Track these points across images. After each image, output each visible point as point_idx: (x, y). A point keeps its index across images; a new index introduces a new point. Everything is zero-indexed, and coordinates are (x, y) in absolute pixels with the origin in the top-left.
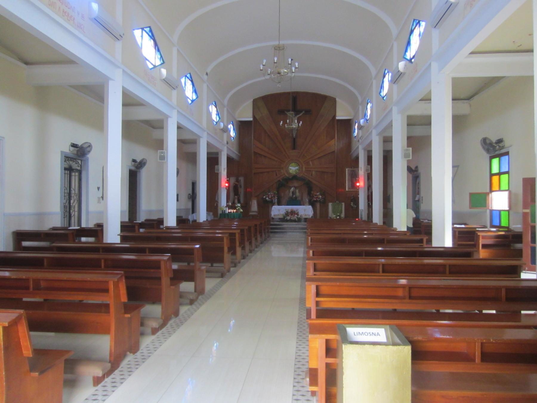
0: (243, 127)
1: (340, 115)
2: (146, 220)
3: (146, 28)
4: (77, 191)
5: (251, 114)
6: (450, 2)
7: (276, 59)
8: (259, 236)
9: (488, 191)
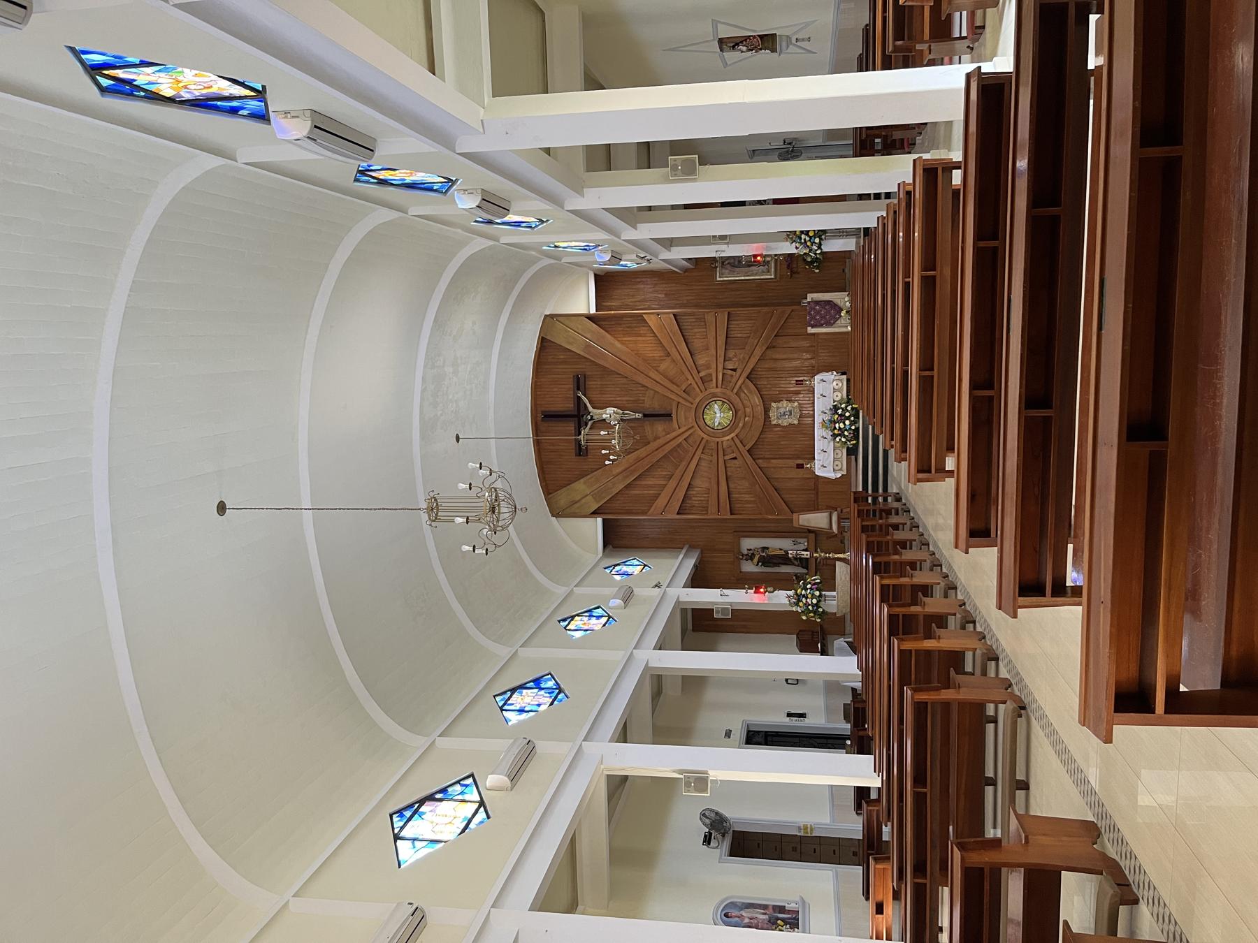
1: (583, 301)
2: (846, 718)
5: (589, 522)
6: (311, 131)
7: (459, 520)
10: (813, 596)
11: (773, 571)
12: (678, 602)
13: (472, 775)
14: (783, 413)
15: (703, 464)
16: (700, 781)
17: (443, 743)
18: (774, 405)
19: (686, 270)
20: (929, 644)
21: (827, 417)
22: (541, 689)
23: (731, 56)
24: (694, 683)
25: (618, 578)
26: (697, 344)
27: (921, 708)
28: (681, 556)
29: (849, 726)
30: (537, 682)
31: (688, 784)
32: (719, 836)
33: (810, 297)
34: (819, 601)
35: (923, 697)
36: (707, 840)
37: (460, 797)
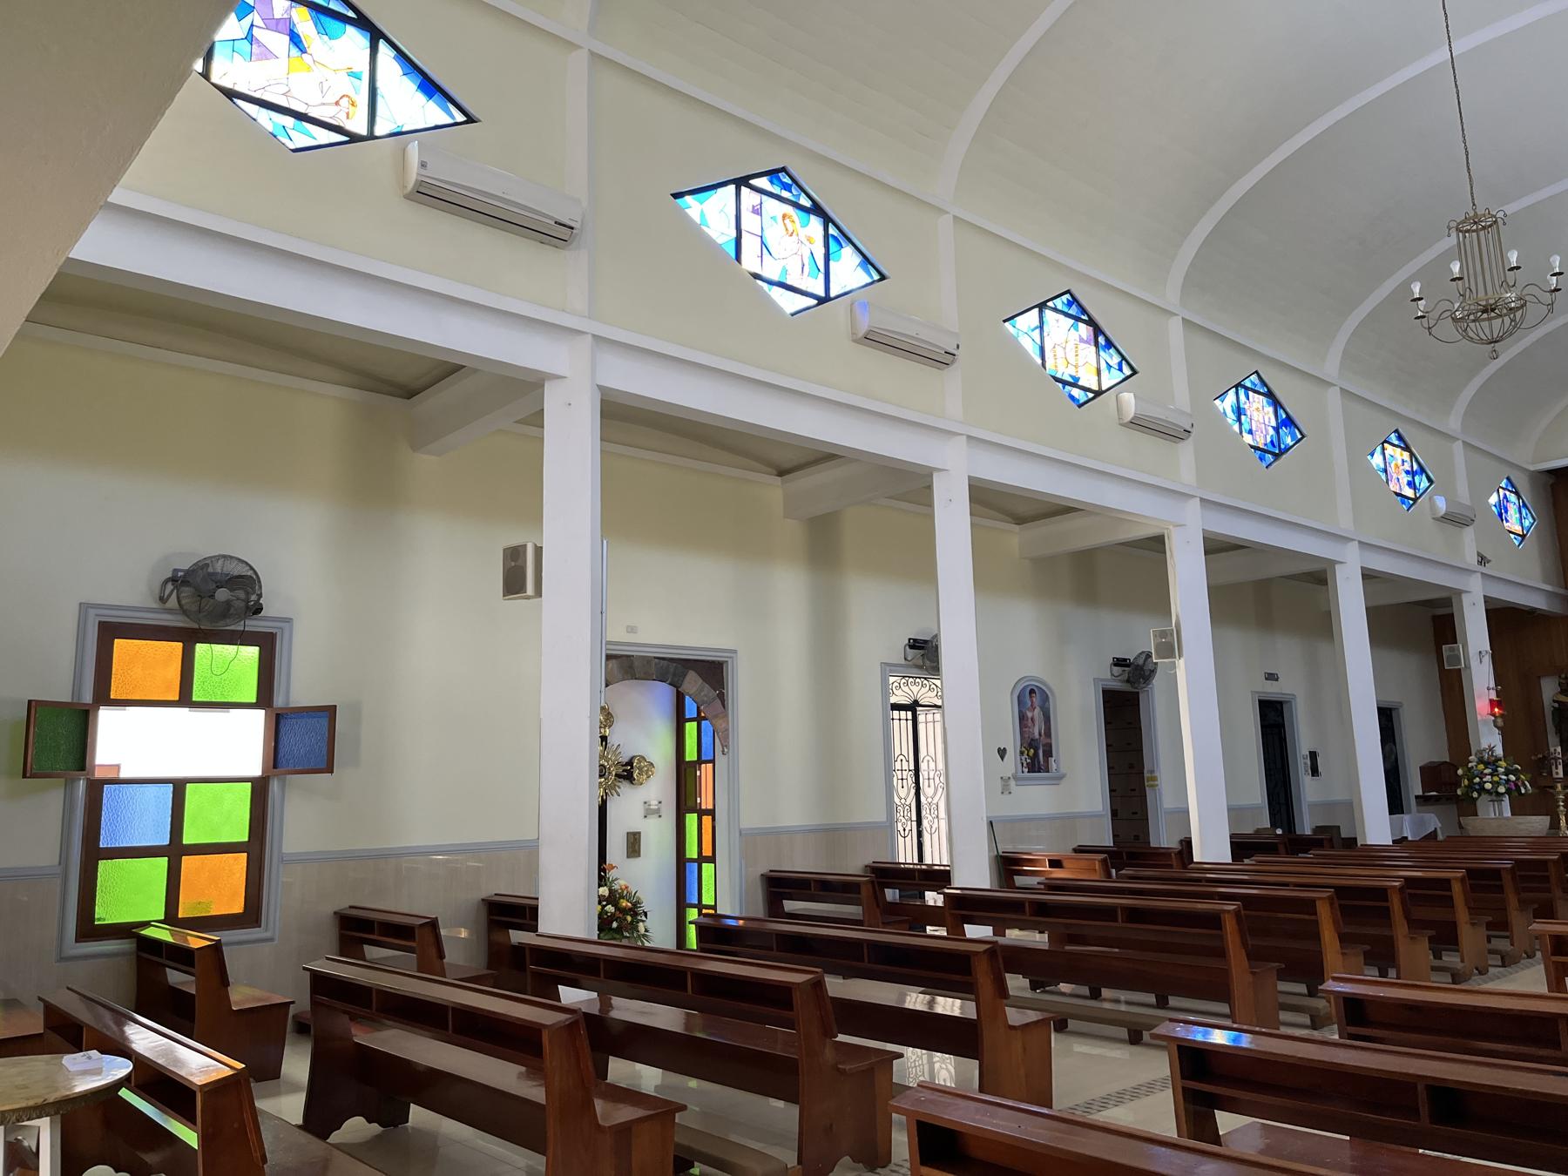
10: (1496, 784)
12: (1459, 593)
13: (1134, 372)
16: (1170, 648)
17: (1175, 327)
20: (1329, 936)
22: (1277, 429)
24: (1324, 625)
25: (1493, 499)
27: (1214, 921)
28: (1548, 588)
29: (1308, 832)
30: (1289, 422)
31: (1163, 634)
32: (1126, 676)
34: (1488, 792)
35: (1230, 925)
36: (1119, 662)
37: (1103, 366)
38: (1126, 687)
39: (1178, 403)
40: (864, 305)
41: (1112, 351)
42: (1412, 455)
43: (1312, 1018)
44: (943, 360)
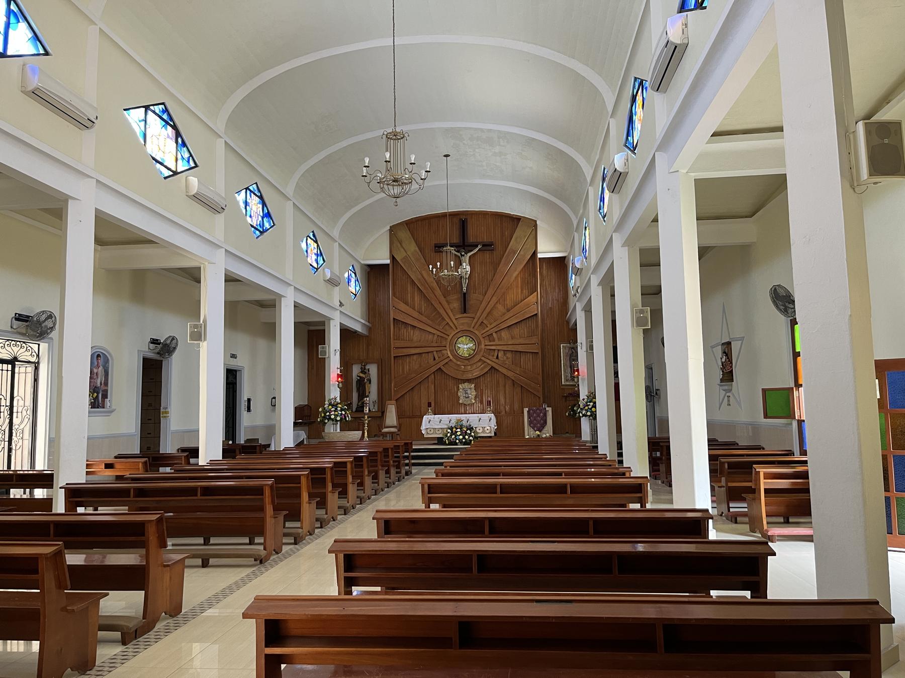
0: (374, 274)
1: (547, 249)
2: (248, 441)
3: (153, 105)
4: (29, 402)
5: (387, 254)
7: (388, 155)
8: (368, 481)
9: (792, 384)
10: (336, 416)
11: (353, 387)
13: (196, 166)
14: (467, 392)
15: (431, 336)
16: (198, 336)
18: (473, 386)
19: (568, 322)
20: (305, 496)
21: (464, 423)
22: (263, 218)
23: (719, 351)
24: (271, 331)
25: (346, 275)
26: (516, 331)
27: (259, 491)
28: (363, 321)
29: (242, 442)
30: (268, 215)
31: (196, 326)
32: (157, 350)
33: (549, 409)
34: (332, 420)
35: (267, 492)
36: (154, 341)
37: (179, 157)
38: (157, 357)
39: (218, 189)
40: (33, 70)
41: (185, 149)
42: (318, 246)
43: (295, 539)
44: (85, 124)
